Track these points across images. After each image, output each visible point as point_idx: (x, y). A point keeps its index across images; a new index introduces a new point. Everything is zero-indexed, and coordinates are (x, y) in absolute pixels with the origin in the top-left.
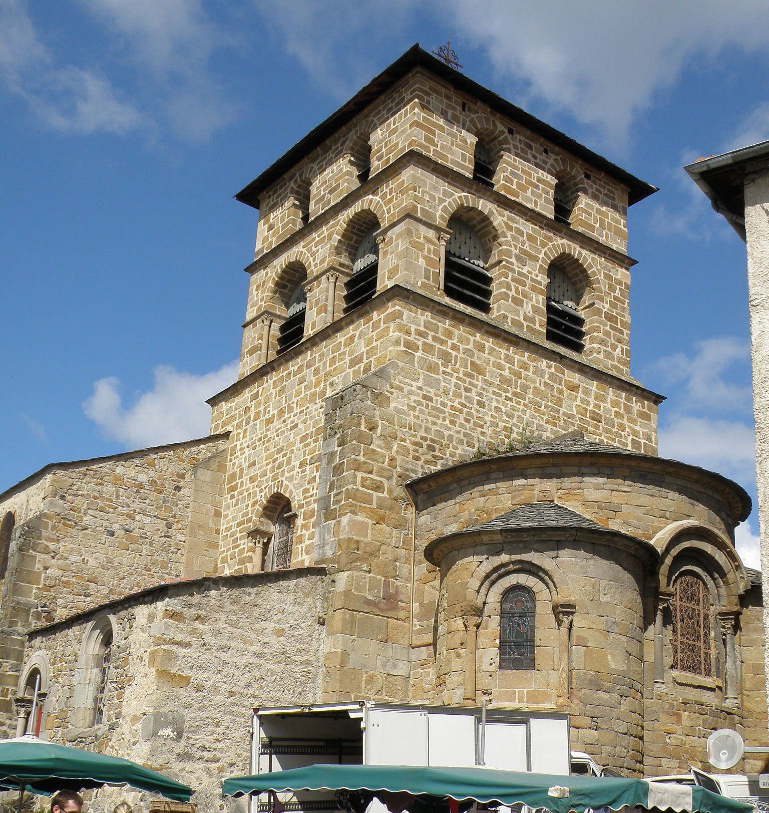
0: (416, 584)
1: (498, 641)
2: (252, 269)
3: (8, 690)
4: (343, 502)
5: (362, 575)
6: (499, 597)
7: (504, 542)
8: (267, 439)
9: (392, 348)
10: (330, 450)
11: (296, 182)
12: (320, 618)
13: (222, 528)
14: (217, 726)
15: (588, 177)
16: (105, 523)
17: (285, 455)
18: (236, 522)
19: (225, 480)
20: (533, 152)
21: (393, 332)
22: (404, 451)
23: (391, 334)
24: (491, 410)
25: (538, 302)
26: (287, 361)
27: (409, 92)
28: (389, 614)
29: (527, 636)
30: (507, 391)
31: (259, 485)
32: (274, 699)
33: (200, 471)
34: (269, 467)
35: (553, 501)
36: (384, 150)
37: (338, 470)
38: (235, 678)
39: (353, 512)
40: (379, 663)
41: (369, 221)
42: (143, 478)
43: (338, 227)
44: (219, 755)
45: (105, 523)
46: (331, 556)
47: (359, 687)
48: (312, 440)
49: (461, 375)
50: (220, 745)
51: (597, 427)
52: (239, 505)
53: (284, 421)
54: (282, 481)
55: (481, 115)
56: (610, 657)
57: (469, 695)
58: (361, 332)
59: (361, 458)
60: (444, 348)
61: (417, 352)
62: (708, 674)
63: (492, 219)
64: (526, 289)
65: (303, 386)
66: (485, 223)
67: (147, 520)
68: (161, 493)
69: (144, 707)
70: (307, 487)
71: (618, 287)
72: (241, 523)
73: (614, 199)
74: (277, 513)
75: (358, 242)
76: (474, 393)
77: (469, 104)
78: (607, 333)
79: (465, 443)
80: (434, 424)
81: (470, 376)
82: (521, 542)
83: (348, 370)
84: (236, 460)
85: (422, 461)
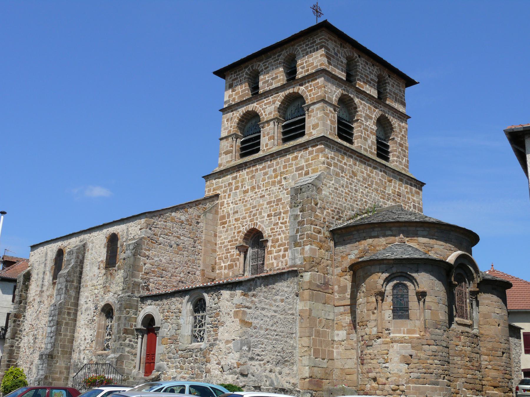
1: (392, 307)
3: (132, 324)
4: (305, 239)
6: (391, 288)
8: (244, 201)
9: (321, 165)
10: (295, 213)
11: (249, 69)
13: (219, 242)
14: (262, 345)
16: (169, 241)
17: (258, 210)
18: (227, 240)
21: (322, 158)
23: (320, 158)
24: (359, 193)
25: (373, 139)
27: (318, 39)
29: (405, 305)
30: (365, 184)
31: (242, 223)
33: (208, 214)
34: (247, 215)
35: (405, 243)
36: (305, 64)
37: (301, 223)
39: (311, 244)
40: (323, 314)
42: (183, 218)
43: (279, 98)
44: (264, 358)
45: (169, 241)
47: (316, 325)
50: (264, 353)
51: (399, 199)
53: (256, 193)
54: (257, 223)
55: (348, 51)
56: (440, 314)
58: (302, 155)
59: (313, 219)
62: (467, 319)
66: (349, 102)
67: (186, 239)
68: (191, 225)
69: (233, 336)
72: (231, 241)
73: (400, 87)
75: (288, 106)
76: (353, 186)
78: (399, 153)
80: (339, 201)
81: (351, 177)
83: (295, 173)
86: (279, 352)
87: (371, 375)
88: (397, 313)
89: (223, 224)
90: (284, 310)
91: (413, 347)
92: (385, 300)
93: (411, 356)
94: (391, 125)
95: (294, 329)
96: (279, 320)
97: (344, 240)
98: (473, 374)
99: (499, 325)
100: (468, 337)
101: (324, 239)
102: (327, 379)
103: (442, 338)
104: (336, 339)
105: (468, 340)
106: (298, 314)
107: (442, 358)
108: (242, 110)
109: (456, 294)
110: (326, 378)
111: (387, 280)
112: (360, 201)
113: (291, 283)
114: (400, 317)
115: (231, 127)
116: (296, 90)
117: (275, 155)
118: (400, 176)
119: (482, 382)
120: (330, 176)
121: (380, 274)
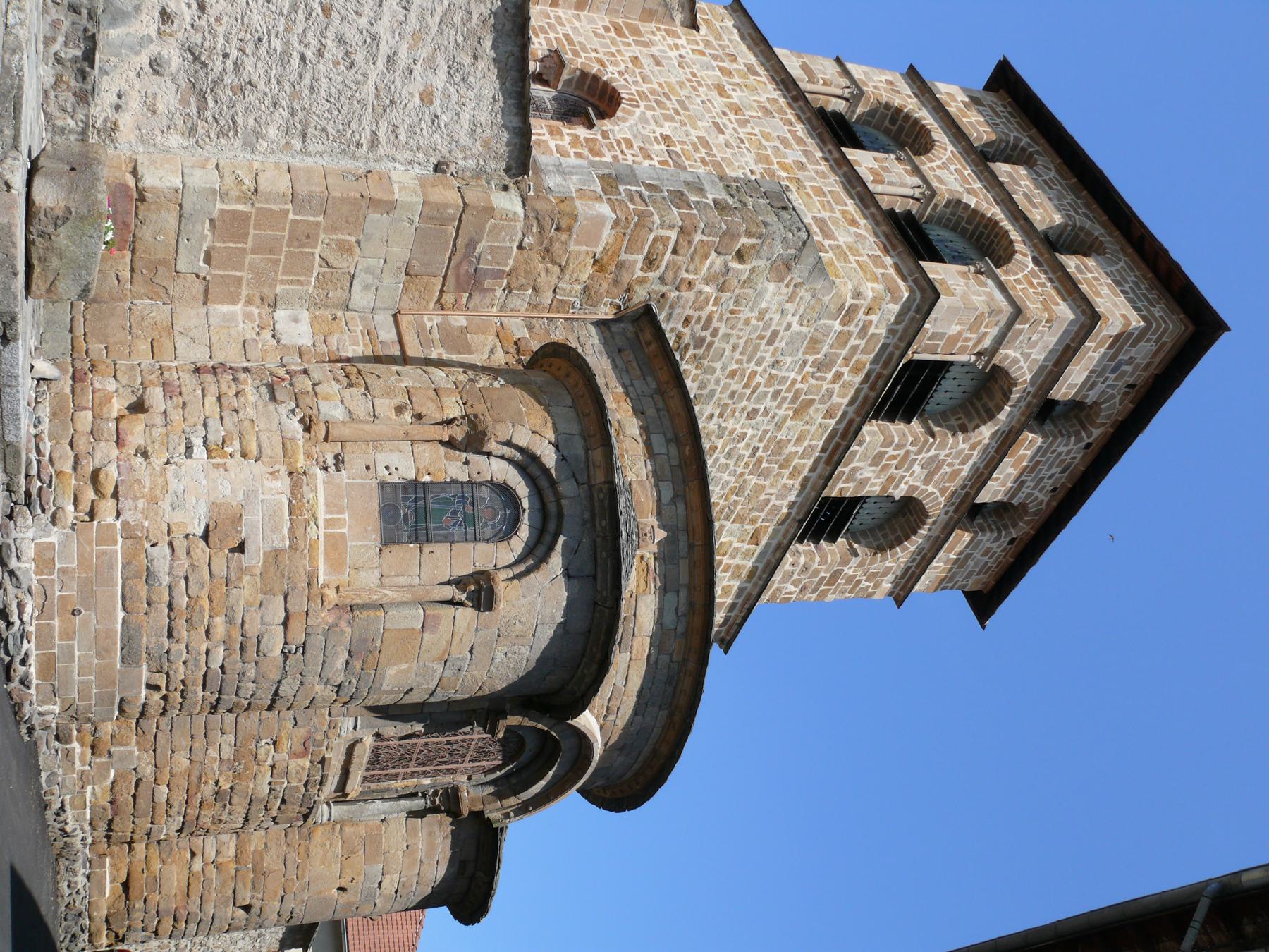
0: (496, 320)
1: (426, 478)
2: (913, 74)
5: (516, 235)
6: (499, 478)
7: (591, 487)
8: (696, 85)
9: (850, 287)
10: (707, 187)
12: (448, 166)
13: (560, 12)
15: (1012, 541)
19: (630, 19)
20: (1057, 475)
21: (872, 289)
22: (700, 303)
23: (869, 285)
24: (742, 427)
25: (874, 485)
26: (809, 121)
27: (1161, 314)
28: (451, 279)
30: (766, 448)
31: (629, 70)
32: (315, 84)
34: (656, 86)
36: (1089, 275)
37: (679, 199)
38: (355, 16)
39: (616, 223)
41: (994, 249)
43: (986, 205)
46: (546, 185)
47: (334, 229)
48: (704, 155)
49: (798, 386)
52: (596, 39)
53: (724, 113)
54: (638, 107)
55: (1114, 408)
56: (404, 666)
57: (334, 431)
58: (865, 238)
59: (698, 237)
60: (839, 362)
61: (840, 323)
62: (365, 779)
63: (990, 424)
64: (893, 470)
65: (777, 143)
70: (635, 146)
71: (872, 584)
72: (570, 42)
73: (978, 574)
74: (586, 97)
76: (769, 404)
77: (1133, 393)
78: (816, 572)
79: (700, 392)
80: (734, 348)
81: (795, 398)
82: (593, 515)
84: (660, 38)
85: (682, 329)
86: (237, 67)
87: (155, 396)
88: (405, 499)
89: (615, 29)
90: (393, 102)
91: (275, 556)
92: (453, 453)
93: (241, 548)
94: (892, 547)
95: (320, 147)
96: (359, 77)
97: (620, 351)
98: (169, 805)
99: (342, 889)
100: (306, 785)
101: (626, 279)
102: (132, 270)
103: (312, 679)
104: (281, 314)
105: (294, 784)
106: (372, 165)
107: (231, 676)
108: (925, 117)
109: (453, 738)
110: (138, 265)
111: (528, 463)
112: (719, 426)
113: (486, 144)
114: (389, 513)
115: (875, 87)
116: (1019, 246)
117: (845, 169)
118: (764, 571)
119: (140, 842)
120: (815, 315)
121: (552, 437)
